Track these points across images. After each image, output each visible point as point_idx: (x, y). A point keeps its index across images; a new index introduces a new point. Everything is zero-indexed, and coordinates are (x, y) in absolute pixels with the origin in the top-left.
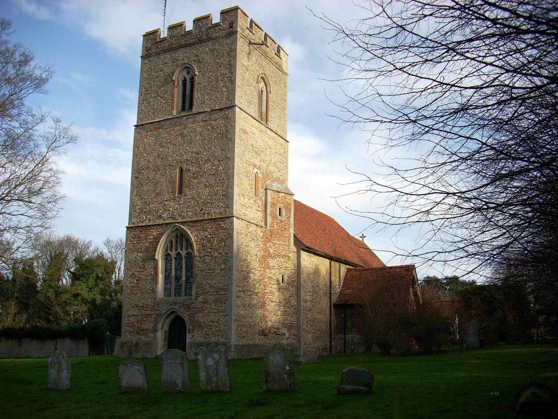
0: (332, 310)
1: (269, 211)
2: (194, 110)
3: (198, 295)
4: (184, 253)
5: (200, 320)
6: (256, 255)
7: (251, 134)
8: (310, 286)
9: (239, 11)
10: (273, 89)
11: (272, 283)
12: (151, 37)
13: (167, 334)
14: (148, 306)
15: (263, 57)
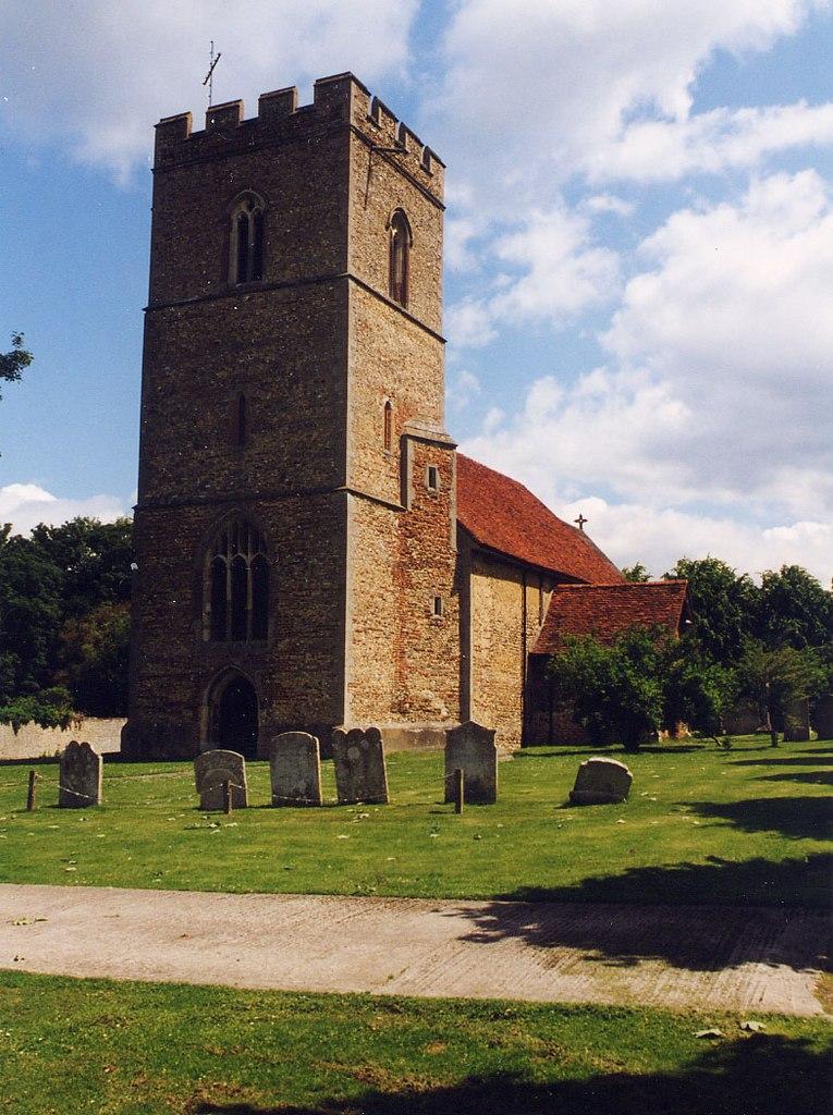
1: (410, 476)
4: (249, 559)
9: (354, 88)
10: (419, 235)
11: (417, 614)
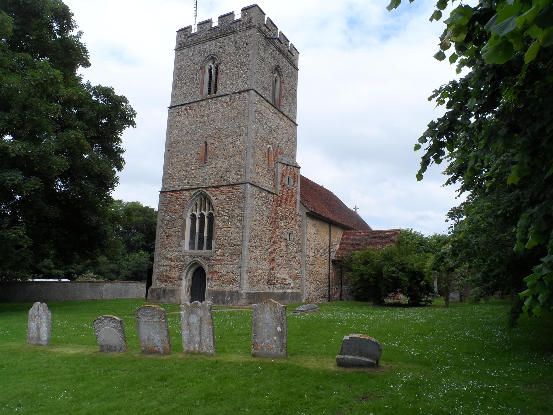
0: (331, 267)
2: (218, 94)
3: (216, 249)
4: (206, 214)
5: (218, 271)
6: (267, 216)
7: (265, 115)
8: (313, 244)
12: (184, 32)
13: (190, 282)
14: (175, 257)
15: (277, 52)
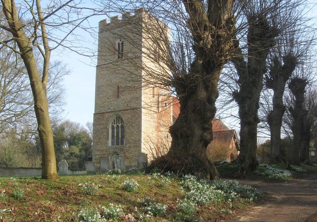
3: (126, 144)
4: (120, 125)
